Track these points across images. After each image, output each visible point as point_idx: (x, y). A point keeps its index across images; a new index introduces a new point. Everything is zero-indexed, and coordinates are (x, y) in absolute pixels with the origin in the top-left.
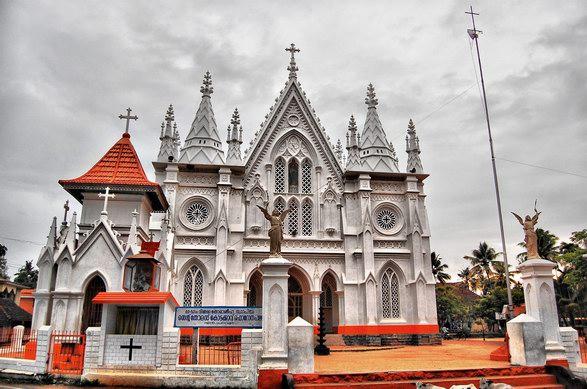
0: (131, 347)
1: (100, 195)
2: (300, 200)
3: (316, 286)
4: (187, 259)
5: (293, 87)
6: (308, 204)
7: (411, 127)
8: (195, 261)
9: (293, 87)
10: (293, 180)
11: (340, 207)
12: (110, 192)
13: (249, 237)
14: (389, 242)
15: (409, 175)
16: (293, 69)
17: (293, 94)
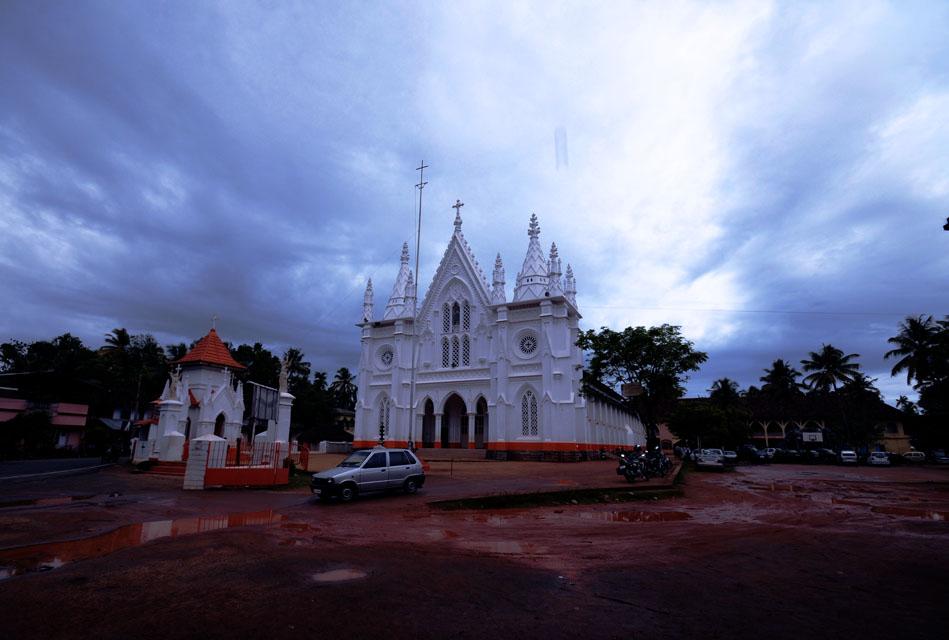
2: (460, 337)
3: (471, 409)
4: (377, 392)
6: (466, 341)
8: (383, 393)
10: (456, 320)
15: (542, 300)
16: (458, 223)
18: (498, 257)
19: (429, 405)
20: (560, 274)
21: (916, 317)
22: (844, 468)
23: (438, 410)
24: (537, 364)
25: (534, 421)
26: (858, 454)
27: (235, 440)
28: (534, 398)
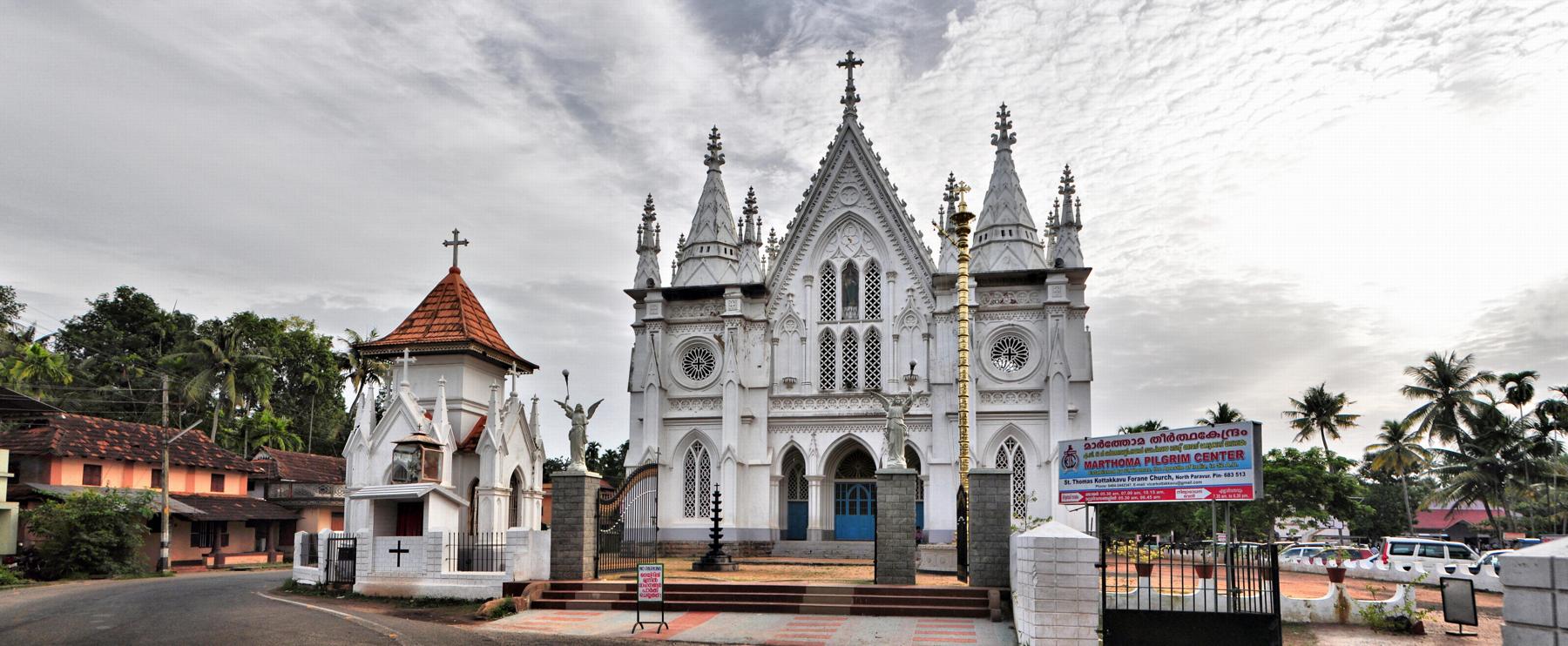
0: (399, 551)
1: (398, 360)
2: (861, 329)
5: (850, 139)
6: (873, 338)
7: (1067, 179)
9: (850, 139)
10: (850, 298)
11: (927, 337)
12: (411, 355)
13: (775, 394)
14: (1010, 392)
16: (850, 99)
17: (849, 147)
18: (1067, 173)
19: (793, 460)
20: (759, 244)
21: (1392, 420)
22: (485, 363)
23: (814, 467)
24: (712, 398)
25: (922, 492)
26: (1273, 522)
27: (1097, 569)
28: (1019, 451)
